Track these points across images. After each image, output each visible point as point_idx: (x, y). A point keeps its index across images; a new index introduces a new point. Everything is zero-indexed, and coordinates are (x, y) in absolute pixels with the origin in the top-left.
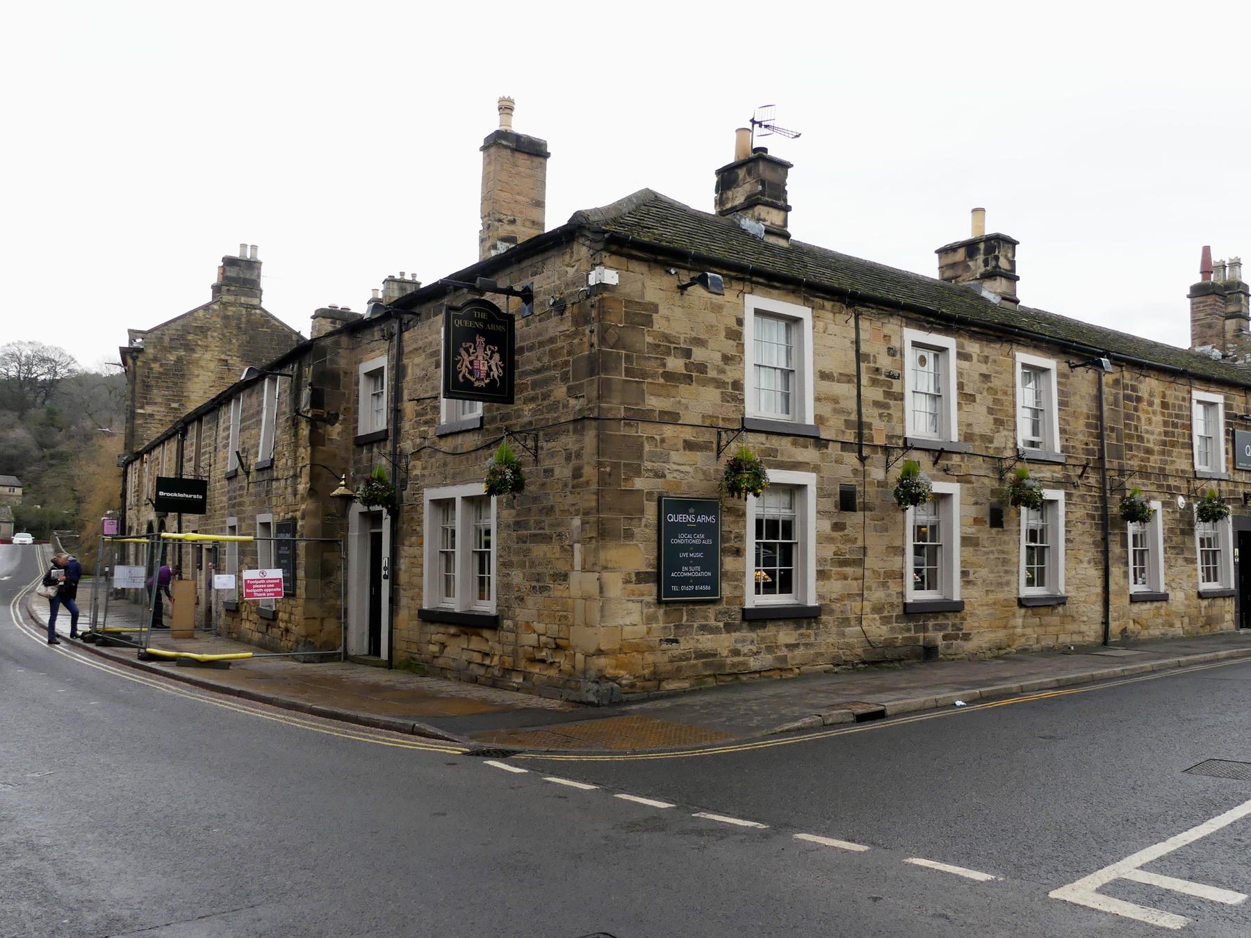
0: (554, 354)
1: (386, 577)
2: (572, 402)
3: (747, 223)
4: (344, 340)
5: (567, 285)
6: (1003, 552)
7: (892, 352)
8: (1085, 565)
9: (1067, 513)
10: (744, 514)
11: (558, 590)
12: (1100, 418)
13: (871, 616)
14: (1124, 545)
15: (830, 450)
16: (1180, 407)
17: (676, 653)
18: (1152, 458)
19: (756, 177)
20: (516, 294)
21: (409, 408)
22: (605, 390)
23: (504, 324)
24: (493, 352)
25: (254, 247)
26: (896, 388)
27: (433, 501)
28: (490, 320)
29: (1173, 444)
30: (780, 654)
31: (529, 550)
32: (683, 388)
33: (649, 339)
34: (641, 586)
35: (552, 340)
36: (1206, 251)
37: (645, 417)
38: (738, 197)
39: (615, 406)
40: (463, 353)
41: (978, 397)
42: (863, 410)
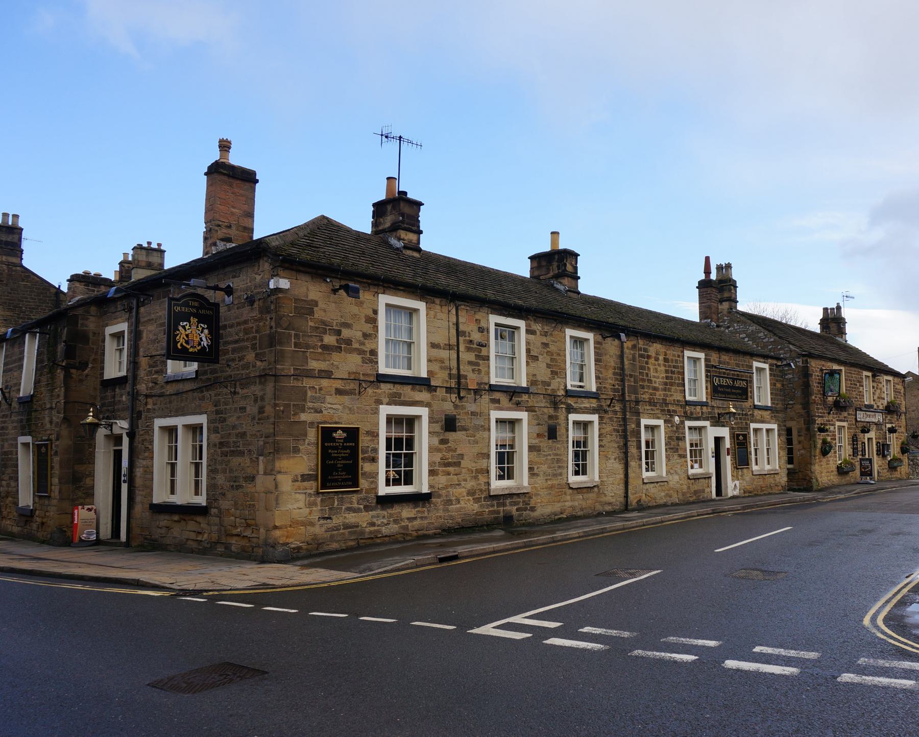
0: (247, 331)
1: (125, 481)
2: (258, 363)
3: (393, 242)
4: (93, 309)
5: (256, 287)
6: (557, 455)
7: (481, 330)
8: (612, 461)
9: (600, 429)
10: (378, 435)
11: (249, 488)
12: (622, 369)
13: (467, 498)
14: (639, 447)
15: (438, 393)
16: (676, 361)
17: (330, 526)
18: (657, 393)
19: (398, 211)
20: (221, 289)
21: (144, 362)
22: (280, 357)
23: (212, 309)
24: (203, 329)
25: (16, 217)
26: (484, 352)
27: (160, 427)
28: (201, 307)
29: (672, 384)
30: (403, 524)
31: (229, 461)
32: (335, 356)
33: (311, 324)
34: (306, 484)
35: (246, 322)
36: (707, 259)
37: (309, 374)
38: (387, 222)
39: (287, 367)
40: (180, 328)
41: (540, 357)
42: (461, 367)
